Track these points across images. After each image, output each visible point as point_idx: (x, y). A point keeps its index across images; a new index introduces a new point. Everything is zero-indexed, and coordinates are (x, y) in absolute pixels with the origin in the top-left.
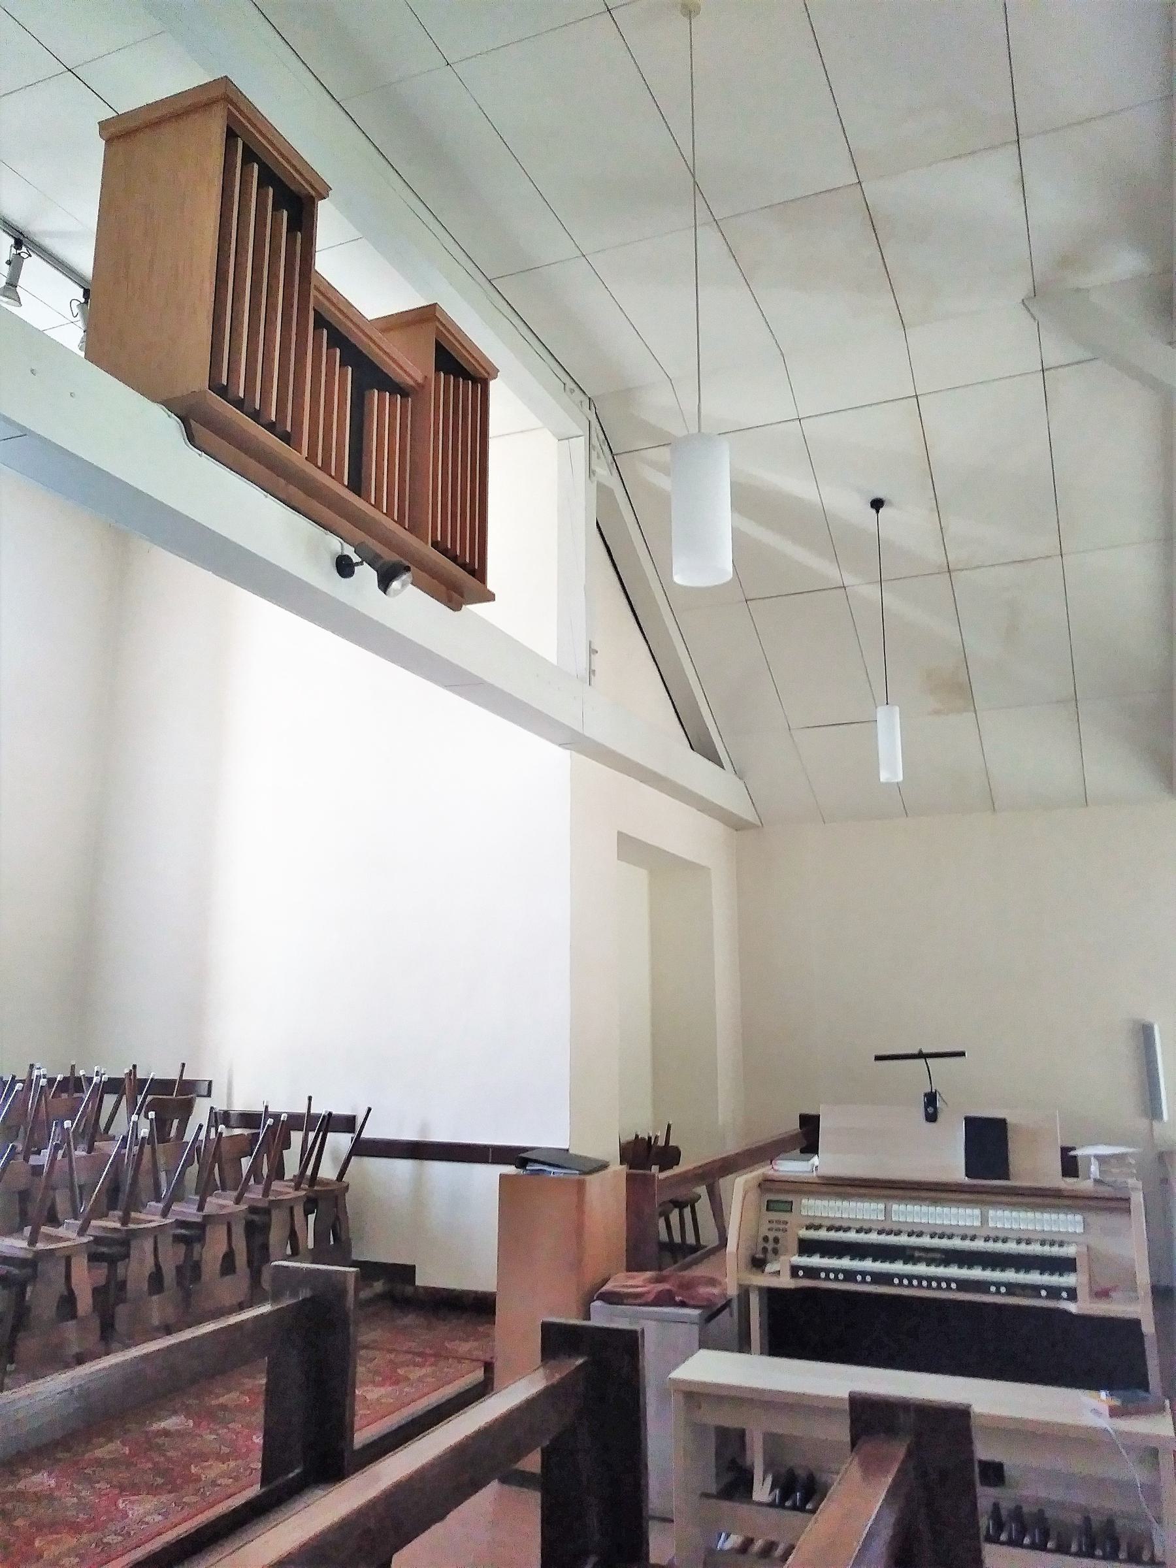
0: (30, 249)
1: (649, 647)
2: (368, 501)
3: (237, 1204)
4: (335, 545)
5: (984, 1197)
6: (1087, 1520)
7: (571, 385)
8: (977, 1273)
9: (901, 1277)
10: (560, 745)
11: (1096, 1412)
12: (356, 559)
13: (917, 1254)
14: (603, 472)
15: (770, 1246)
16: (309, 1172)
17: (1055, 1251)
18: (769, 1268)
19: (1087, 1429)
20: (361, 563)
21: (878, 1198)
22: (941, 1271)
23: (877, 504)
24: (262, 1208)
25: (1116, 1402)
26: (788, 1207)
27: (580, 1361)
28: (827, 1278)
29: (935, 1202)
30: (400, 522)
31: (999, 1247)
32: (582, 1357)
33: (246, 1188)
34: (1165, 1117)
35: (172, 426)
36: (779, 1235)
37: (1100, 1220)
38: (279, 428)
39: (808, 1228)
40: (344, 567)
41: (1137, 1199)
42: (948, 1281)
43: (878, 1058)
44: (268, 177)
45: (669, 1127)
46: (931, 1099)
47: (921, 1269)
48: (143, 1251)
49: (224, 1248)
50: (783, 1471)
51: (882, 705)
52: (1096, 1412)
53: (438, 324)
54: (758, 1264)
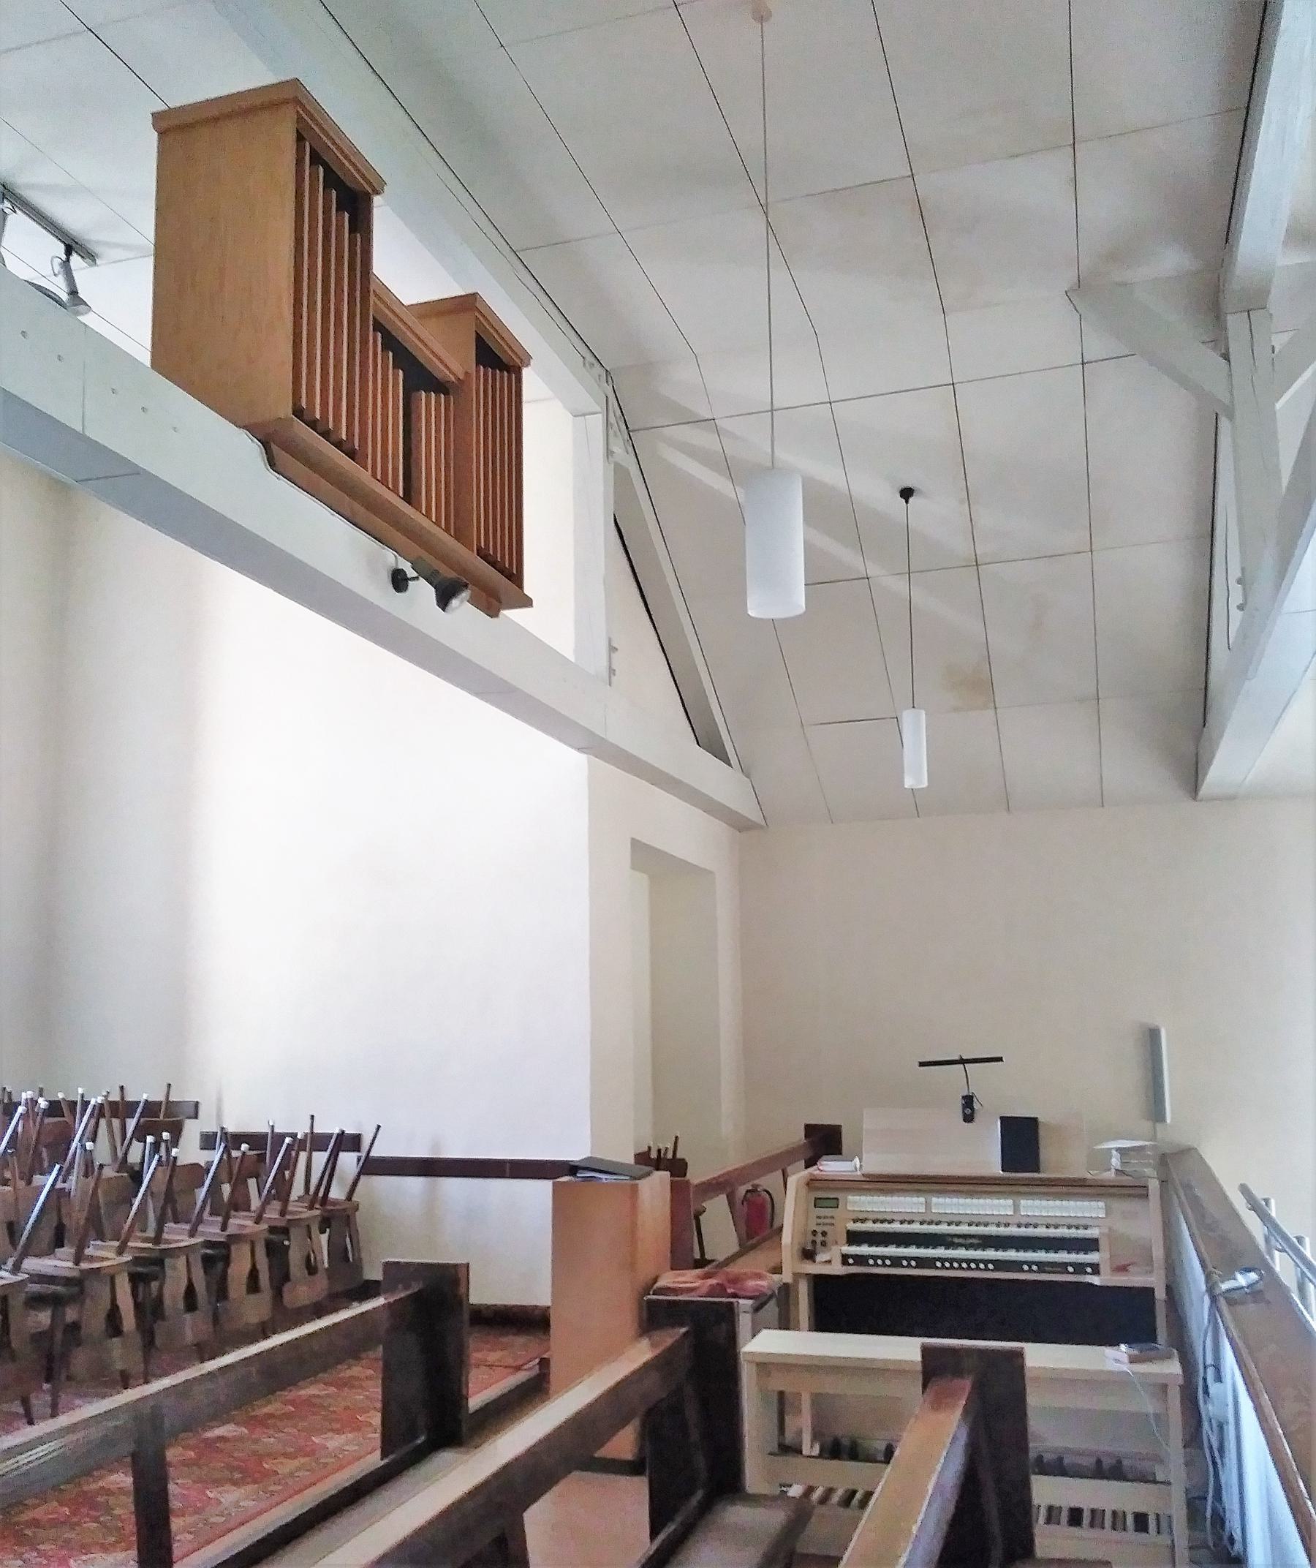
0: (15, 205)
1: (658, 636)
2: (418, 508)
3: (222, 1231)
4: (390, 558)
5: (1014, 1188)
6: (1099, 1462)
7: (590, 358)
8: (1011, 1255)
9: (943, 1260)
10: (579, 750)
11: (1117, 1361)
12: (411, 573)
13: (956, 1240)
14: (619, 449)
15: (819, 1238)
16: (321, 1194)
17: (1081, 1233)
18: (819, 1258)
19: (1111, 1372)
20: (416, 578)
21: (919, 1192)
22: (978, 1254)
23: (907, 493)
24: (281, 1228)
25: (1136, 1352)
26: (835, 1203)
27: (683, 1330)
28: (876, 1265)
29: (971, 1194)
30: (447, 530)
31: (1030, 1232)
32: (684, 1327)
33: (200, 1220)
34: (1168, 1120)
35: (251, 449)
36: (825, 1228)
37: (1121, 1206)
38: (333, 437)
39: (855, 1221)
40: (399, 582)
41: (1154, 1185)
42: (986, 1262)
43: (922, 1064)
44: (332, 180)
45: (677, 1138)
46: (968, 1101)
47: (961, 1253)
48: (174, 1268)
49: (248, 1267)
50: (829, 1440)
51: (907, 708)
52: (1117, 1361)
53: (477, 314)
54: (808, 1255)
